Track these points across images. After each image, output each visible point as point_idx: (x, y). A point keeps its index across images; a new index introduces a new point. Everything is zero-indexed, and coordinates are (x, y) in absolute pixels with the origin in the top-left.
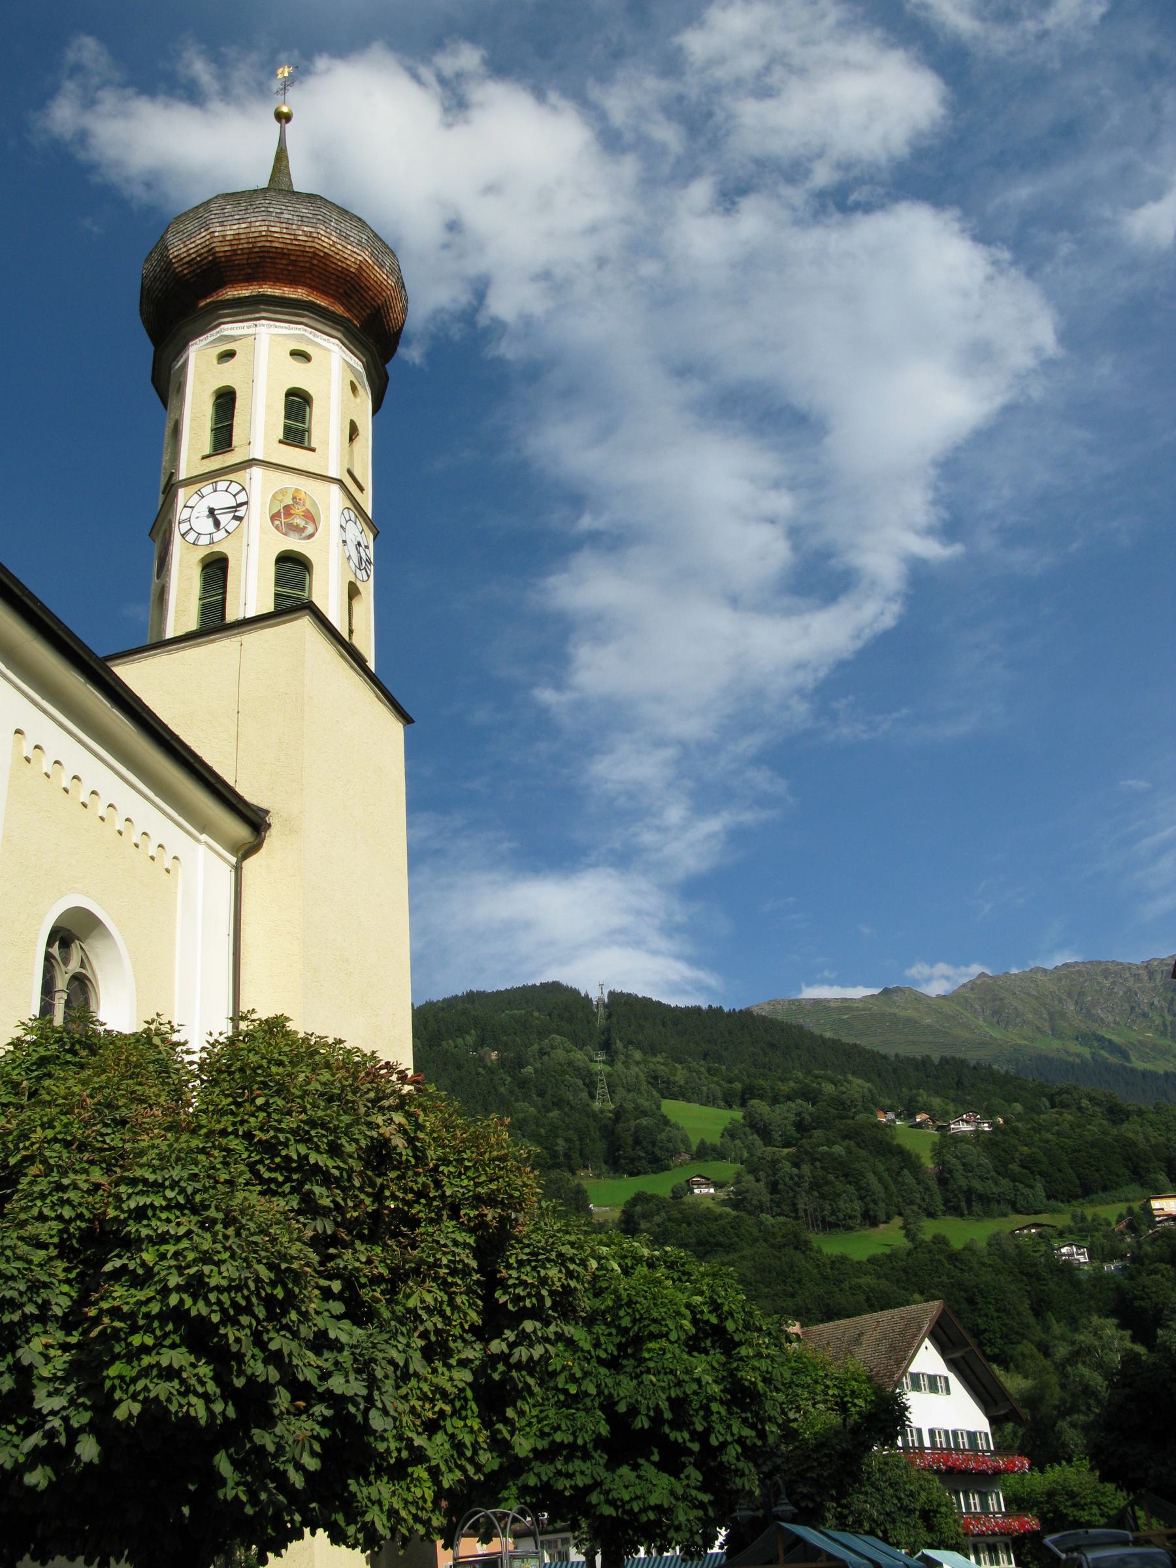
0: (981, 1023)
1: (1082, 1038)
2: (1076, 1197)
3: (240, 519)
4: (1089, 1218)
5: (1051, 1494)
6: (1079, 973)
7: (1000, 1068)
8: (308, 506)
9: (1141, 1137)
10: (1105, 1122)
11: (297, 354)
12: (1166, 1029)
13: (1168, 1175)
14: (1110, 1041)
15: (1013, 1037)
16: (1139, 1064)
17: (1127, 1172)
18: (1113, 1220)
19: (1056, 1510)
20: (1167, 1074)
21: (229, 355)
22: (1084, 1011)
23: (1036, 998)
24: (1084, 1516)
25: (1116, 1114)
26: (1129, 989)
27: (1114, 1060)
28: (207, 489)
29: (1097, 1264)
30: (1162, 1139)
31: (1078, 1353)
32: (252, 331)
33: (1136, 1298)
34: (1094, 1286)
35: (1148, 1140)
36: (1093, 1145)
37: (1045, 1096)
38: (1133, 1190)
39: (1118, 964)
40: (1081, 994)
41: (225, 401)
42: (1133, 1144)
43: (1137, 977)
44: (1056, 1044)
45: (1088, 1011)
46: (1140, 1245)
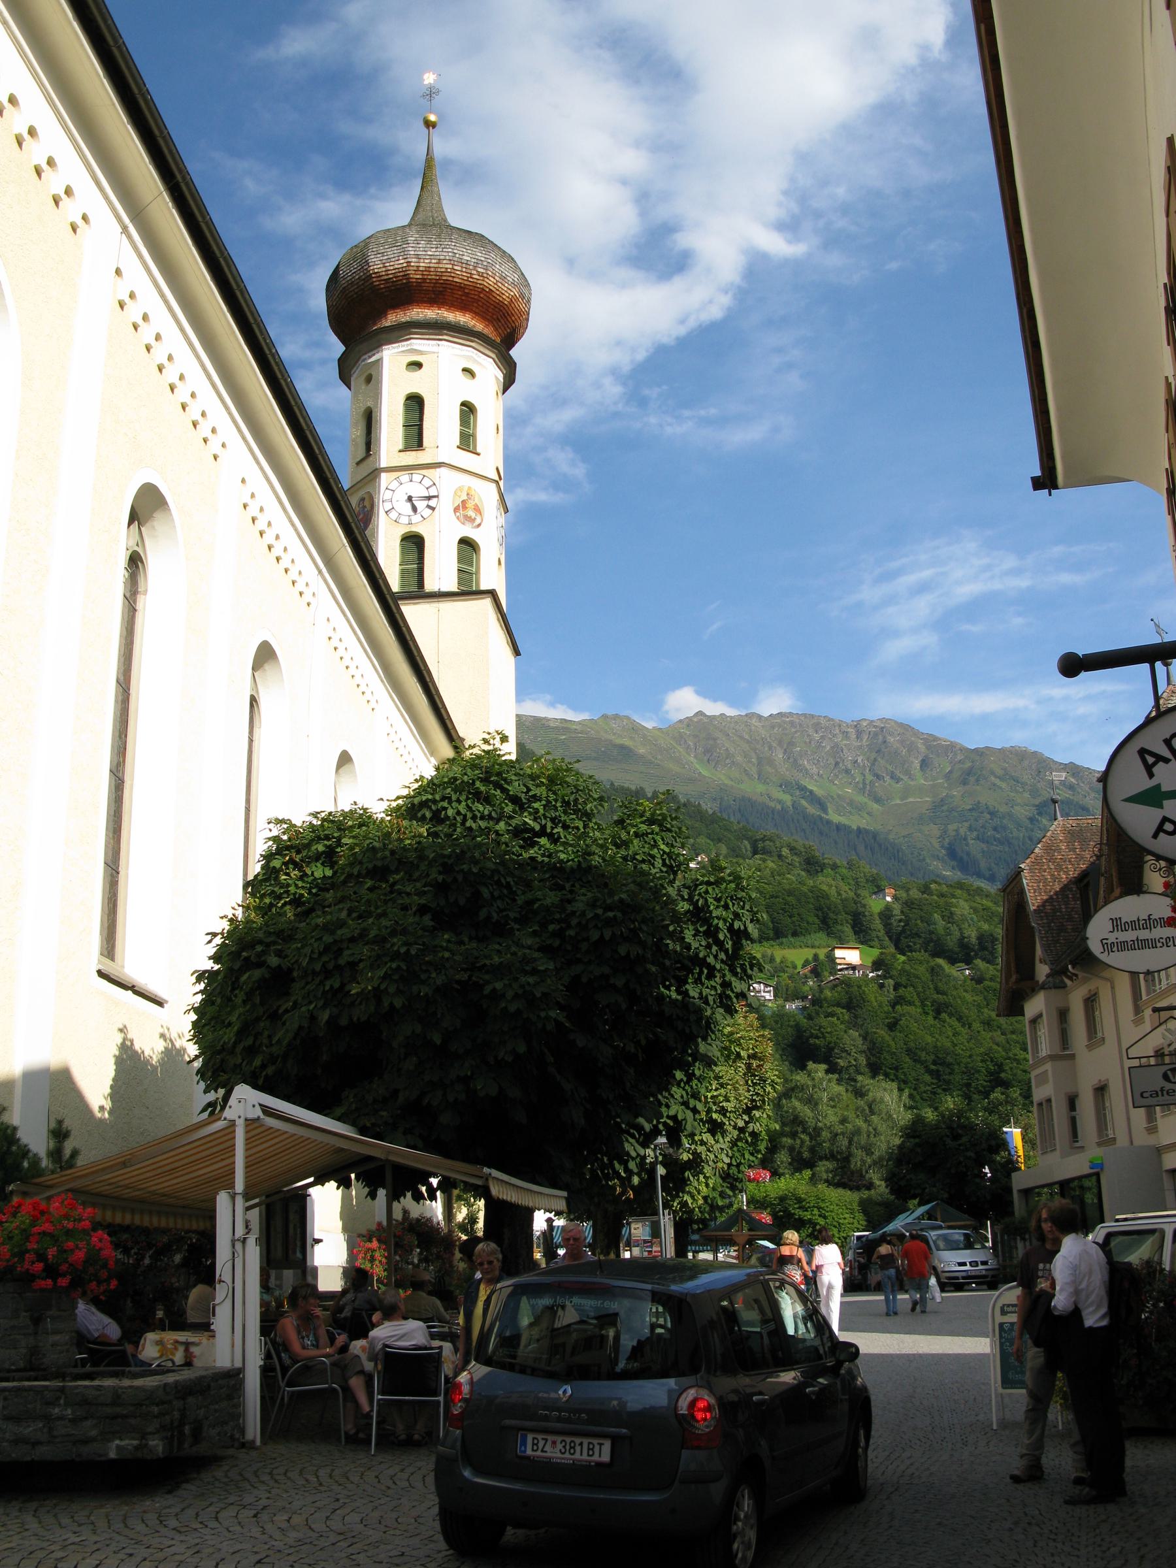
0: (692, 759)
1: (785, 785)
2: (768, 939)
3: (433, 509)
4: (778, 960)
5: (782, 1199)
6: (792, 723)
7: (708, 807)
8: (477, 501)
9: (833, 892)
10: (803, 873)
11: (468, 371)
12: (864, 788)
13: (853, 928)
14: (811, 792)
15: (718, 776)
16: (835, 818)
17: (817, 921)
18: (799, 964)
19: (786, 1210)
20: (859, 830)
21: (418, 365)
22: (791, 760)
23: (748, 742)
24: (807, 1216)
25: (813, 865)
26: (836, 745)
27: (812, 810)
28: (405, 477)
29: (780, 1002)
30: (851, 894)
31: (793, 1089)
32: (435, 349)
33: (812, 1036)
34: (776, 1022)
35: (839, 894)
36: (790, 893)
37: (747, 839)
38: (820, 937)
39: (830, 720)
40: (791, 744)
41: (415, 403)
42: (826, 896)
43: (846, 735)
44: (761, 788)
45: (795, 760)
46: (821, 990)
